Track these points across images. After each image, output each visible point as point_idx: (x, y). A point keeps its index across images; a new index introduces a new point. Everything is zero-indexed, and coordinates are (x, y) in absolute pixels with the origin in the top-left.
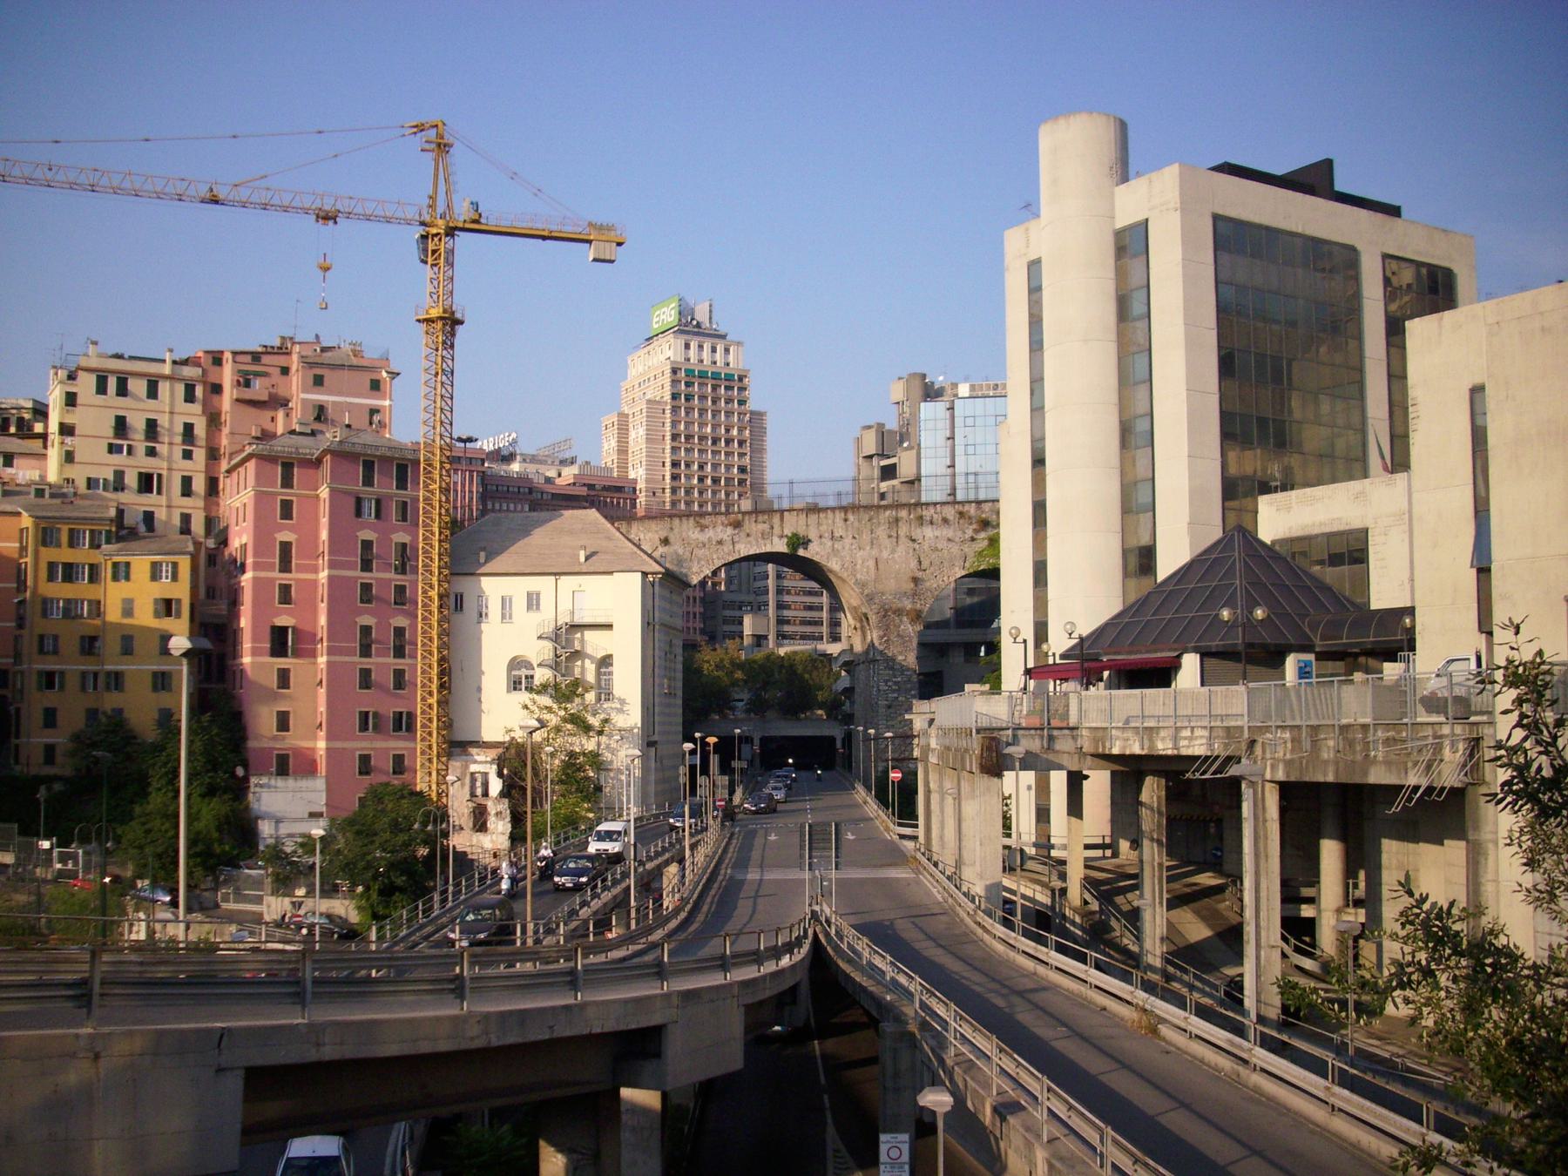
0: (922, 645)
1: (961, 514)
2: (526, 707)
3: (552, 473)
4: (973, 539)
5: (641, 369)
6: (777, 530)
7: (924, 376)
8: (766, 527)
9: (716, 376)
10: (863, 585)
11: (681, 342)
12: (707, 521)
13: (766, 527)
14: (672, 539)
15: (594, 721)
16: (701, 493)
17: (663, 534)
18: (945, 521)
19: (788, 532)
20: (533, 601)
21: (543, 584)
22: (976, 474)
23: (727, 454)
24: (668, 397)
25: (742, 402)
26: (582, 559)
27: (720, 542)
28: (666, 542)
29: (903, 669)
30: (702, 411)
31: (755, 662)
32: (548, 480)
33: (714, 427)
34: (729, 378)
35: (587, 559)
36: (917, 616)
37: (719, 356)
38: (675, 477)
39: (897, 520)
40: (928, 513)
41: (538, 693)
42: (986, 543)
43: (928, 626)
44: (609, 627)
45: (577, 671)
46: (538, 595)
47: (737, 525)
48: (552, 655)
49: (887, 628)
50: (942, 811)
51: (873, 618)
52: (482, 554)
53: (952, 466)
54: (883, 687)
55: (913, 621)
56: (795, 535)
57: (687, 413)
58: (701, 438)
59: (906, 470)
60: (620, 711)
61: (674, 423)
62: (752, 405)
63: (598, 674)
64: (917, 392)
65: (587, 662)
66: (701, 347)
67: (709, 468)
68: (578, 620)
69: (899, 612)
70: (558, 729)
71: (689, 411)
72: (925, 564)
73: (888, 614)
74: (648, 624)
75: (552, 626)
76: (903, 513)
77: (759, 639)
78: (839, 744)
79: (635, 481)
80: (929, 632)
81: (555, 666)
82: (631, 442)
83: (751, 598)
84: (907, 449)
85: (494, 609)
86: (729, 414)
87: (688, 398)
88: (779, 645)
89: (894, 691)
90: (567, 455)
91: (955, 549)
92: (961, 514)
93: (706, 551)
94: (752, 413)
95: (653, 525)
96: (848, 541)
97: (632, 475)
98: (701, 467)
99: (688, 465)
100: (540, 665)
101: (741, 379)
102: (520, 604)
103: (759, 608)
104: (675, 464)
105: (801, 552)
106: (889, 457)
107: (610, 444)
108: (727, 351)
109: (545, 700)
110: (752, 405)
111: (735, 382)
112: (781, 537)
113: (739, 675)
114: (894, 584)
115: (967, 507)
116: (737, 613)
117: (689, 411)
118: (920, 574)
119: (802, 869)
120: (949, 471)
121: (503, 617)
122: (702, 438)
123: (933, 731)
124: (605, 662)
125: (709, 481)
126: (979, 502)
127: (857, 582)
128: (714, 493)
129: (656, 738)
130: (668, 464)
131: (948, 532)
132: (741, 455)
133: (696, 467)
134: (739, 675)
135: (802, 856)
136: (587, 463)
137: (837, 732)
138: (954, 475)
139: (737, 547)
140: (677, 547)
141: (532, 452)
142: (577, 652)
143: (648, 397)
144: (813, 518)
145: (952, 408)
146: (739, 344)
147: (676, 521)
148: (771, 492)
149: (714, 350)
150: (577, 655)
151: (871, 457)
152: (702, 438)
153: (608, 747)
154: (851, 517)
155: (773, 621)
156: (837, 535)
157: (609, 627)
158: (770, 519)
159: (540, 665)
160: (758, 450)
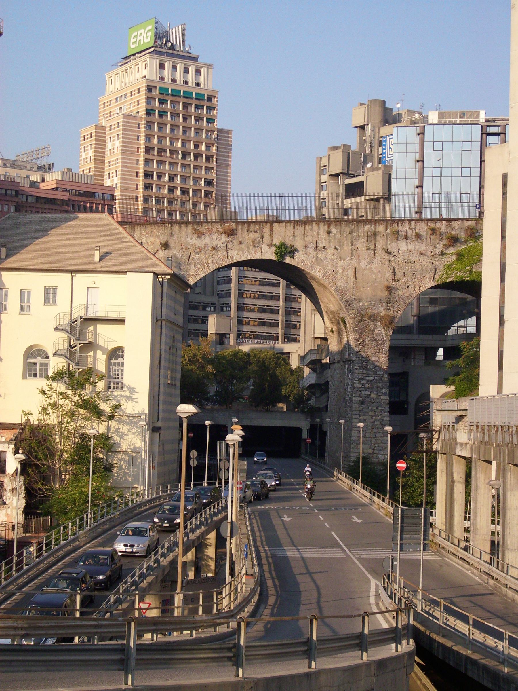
0: (393, 349)
1: (433, 231)
2: (43, 392)
3: (36, 177)
4: (443, 254)
5: (118, 85)
6: (267, 240)
7: (384, 102)
8: (257, 235)
9: (187, 95)
10: (342, 292)
11: (155, 62)
12: (203, 228)
13: (257, 235)
14: (172, 245)
15: (105, 407)
16: (170, 202)
17: (164, 239)
18: (418, 236)
19: (276, 241)
20: (50, 296)
21: (60, 281)
22: (449, 194)
23: (195, 167)
24: (143, 113)
25: (210, 121)
26: (97, 259)
27: (215, 248)
28: (166, 246)
29: (376, 369)
30: (174, 127)
31: (224, 357)
32: (33, 184)
33: (184, 142)
34: (199, 97)
35: (101, 258)
36: (389, 321)
37: (191, 77)
38: (147, 187)
39: (375, 234)
40: (403, 228)
41: (53, 379)
42: (454, 257)
43: (398, 331)
44: (122, 321)
45: (90, 360)
46: (55, 289)
47: (231, 233)
48: (66, 346)
49: (363, 331)
50: (232, 490)
51: (350, 322)
52: (4, 250)
53: (420, 186)
54: (357, 385)
55: (386, 326)
56: (283, 244)
57: (160, 128)
58: (172, 152)
59: (373, 185)
60: (129, 398)
61: (148, 138)
62: (220, 123)
63: (109, 364)
64: (377, 115)
65: (99, 353)
66: (174, 67)
67: (178, 180)
68: (91, 314)
69: (373, 317)
70: (72, 414)
71: (162, 126)
72: (399, 274)
73: (365, 319)
74: (157, 320)
75: (67, 320)
76: (381, 228)
77: (222, 338)
78: (305, 435)
79: (112, 189)
80: (400, 336)
81: (70, 355)
82: (108, 153)
83: (214, 299)
84: (373, 169)
85: (13, 301)
86: (198, 131)
87: (162, 114)
88: (239, 344)
89: (366, 389)
90: (45, 162)
91: (426, 262)
92: (433, 231)
93: (203, 254)
94: (219, 130)
95: (155, 230)
96: (330, 251)
97: (108, 183)
98: (171, 179)
99: (159, 177)
100: (55, 354)
101: (210, 99)
102: (37, 298)
103: (221, 309)
104: (148, 175)
105: (288, 260)
106: (353, 176)
107: (88, 154)
108: (198, 72)
109: (60, 387)
110: (220, 123)
111: (205, 102)
112: (270, 245)
113: (210, 369)
114: (370, 292)
115: (438, 224)
116: (202, 313)
117: (162, 126)
118: (394, 284)
119: (394, 550)
120: (417, 191)
121: (22, 309)
122: (173, 152)
123: (461, 426)
124: (116, 353)
125: (178, 192)
126: (449, 220)
127: (337, 289)
128: (183, 203)
129: (159, 424)
130: (141, 175)
131: (421, 247)
132: (208, 169)
133: (167, 178)
134: (210, 369)
135: (394, 538)
136: (69, 170)
137: (303, 424)
138: (422, 195)
139: (231, 253)
140: (176, 251)
141: (12, 157)
142: (90, 343)
143: (125, 111)
144: (300, 229)
145: (422, 134)
146: (209, 66)
147: (176, 227)
148: (233, 205)
149: (186, 71)
150: (90, 346)
151: (337, 175)
152: (173, 152)
153: (117, 430)
154: (333, 230)
155: (235, 322)
156: (320, 245)
157: (122, 321)
158: (261, 229)
159: (55, 354)
160: (224, 165)
